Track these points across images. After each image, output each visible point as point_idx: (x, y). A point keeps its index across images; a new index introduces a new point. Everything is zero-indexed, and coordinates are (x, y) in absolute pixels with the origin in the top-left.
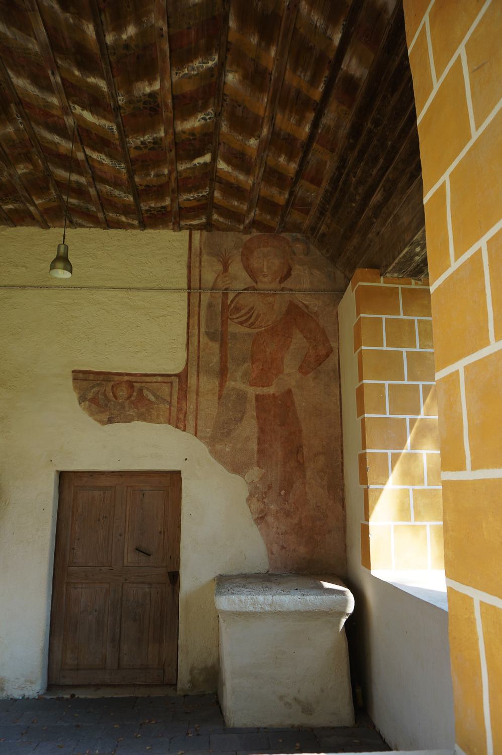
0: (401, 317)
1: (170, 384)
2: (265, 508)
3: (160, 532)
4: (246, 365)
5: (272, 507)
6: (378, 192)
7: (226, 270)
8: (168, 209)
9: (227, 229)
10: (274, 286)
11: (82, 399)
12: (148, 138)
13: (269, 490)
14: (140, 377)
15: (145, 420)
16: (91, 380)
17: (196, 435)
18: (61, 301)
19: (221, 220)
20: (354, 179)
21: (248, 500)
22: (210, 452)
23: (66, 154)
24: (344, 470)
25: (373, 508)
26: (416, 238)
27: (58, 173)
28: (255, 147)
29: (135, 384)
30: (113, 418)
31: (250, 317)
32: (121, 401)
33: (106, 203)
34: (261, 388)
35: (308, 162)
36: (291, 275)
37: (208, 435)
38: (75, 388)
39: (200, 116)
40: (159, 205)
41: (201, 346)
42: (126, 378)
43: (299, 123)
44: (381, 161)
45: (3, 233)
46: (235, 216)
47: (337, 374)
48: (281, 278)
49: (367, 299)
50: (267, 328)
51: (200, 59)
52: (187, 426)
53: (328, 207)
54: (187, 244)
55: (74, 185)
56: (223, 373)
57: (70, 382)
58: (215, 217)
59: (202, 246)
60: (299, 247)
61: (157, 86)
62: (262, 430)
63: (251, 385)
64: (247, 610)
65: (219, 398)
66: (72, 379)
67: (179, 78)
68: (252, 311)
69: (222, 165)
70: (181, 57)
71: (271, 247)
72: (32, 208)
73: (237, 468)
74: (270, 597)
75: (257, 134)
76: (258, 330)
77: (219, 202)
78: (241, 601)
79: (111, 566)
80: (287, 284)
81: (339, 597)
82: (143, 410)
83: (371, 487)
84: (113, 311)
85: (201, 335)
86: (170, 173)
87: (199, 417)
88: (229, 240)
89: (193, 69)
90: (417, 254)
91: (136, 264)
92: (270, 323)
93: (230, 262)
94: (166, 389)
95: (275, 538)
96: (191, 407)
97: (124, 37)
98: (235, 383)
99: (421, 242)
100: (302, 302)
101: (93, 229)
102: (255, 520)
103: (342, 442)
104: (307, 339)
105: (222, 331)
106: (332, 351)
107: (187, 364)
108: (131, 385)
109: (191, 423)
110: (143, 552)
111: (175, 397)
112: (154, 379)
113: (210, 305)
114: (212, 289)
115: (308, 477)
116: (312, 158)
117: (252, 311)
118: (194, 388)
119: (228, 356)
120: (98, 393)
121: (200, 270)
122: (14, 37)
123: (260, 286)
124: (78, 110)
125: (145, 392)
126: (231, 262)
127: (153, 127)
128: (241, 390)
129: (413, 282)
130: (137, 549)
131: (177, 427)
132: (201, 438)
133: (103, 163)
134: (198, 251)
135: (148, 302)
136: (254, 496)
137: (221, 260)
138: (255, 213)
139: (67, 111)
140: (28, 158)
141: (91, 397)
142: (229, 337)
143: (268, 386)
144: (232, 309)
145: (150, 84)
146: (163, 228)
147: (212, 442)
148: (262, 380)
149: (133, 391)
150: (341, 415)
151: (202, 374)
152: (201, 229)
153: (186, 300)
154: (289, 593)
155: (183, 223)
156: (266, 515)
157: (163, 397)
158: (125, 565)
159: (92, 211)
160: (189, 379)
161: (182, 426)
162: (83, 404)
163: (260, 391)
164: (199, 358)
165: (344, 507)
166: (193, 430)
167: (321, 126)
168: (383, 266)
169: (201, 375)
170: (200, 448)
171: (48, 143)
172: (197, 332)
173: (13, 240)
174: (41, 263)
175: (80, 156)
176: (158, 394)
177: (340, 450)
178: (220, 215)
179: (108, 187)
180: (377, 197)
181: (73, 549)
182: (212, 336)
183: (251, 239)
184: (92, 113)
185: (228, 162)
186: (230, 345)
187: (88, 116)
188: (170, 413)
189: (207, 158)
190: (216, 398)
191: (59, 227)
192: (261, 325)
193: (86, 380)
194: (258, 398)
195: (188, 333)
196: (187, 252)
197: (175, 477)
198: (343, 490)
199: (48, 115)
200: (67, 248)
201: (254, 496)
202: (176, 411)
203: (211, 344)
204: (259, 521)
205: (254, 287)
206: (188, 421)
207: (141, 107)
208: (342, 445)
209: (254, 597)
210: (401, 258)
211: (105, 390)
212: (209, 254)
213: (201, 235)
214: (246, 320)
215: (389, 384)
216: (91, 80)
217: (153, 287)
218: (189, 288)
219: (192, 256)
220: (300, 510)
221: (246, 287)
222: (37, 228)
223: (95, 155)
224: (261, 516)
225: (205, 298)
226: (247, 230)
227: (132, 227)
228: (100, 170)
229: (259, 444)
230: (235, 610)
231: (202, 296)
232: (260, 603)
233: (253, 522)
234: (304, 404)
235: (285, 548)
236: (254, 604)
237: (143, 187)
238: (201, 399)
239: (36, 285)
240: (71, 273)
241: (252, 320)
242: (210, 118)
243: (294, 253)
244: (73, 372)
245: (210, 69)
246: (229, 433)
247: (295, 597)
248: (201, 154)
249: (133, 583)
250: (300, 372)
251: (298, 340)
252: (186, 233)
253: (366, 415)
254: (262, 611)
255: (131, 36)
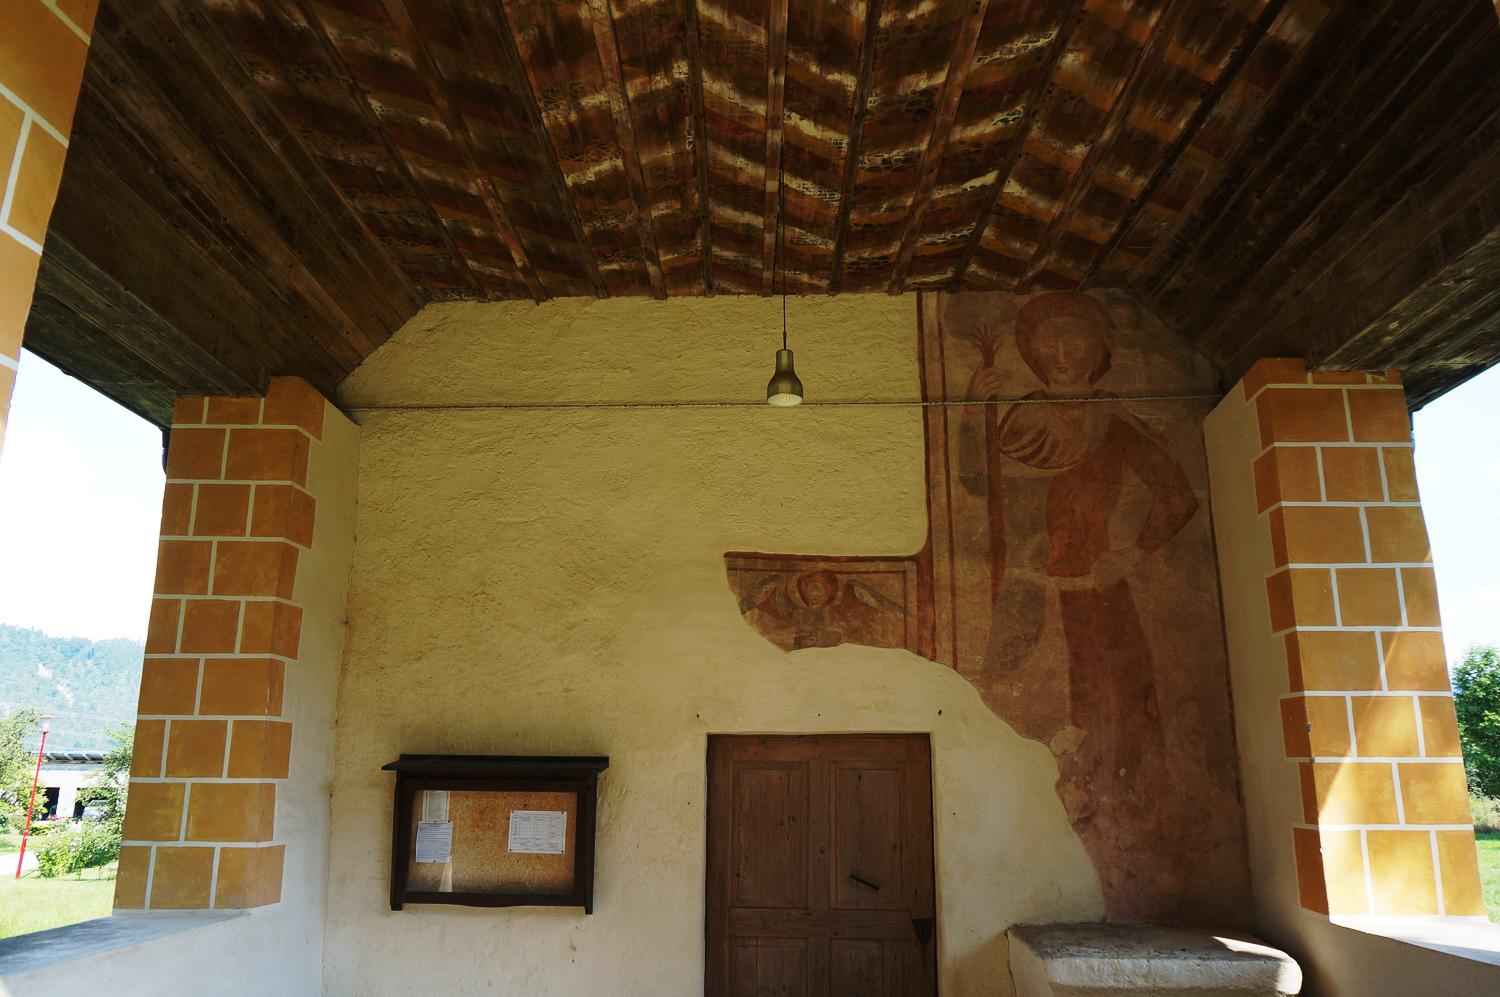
0: (1351, 443)
1: (901, 575)
2: (1092, 801)
3: (894, 847)
4: (1038, 538)
5: (1105, 799)
6: (1309, 223)
7: (988, 362)
8: (891, 260)
9: (990, 286)
10: (1078, 388)
11: (746, 605)
12: (897, 154)
13: (1096, 767)
14: (846, 564)
15: (860, 641)
16: (761, 570)
17: (955, 667)
18: (697, 428)
19: (981, 272)
20: (1257, 201)
21: (1058, 786)
22: (984, 698)
23: (747, 184)
24: (1237, 727)
25: (1324, 799)
26: (1395, 308)
27: (721, 212)
28: (1080, 157)
29: (839, 576)
30: (804, 638)
31: (1041, 448)
32: (815, 606)
33: (788, 254)
34: (1070, 578)
35: (1170, 174)
36: (1110, 366)
37: (979, 667)
38: (733, 585)
39: (1000, 116)
40: (877, 254)
41: (953, 503)
42: (822, 565)
43: (1171, 117)
44: (1322, 173)
45: (587, 309)
46: (1007, 265)
47: (1210, 548)
48: (1093, 373)
49: (1276, 416)
50: (1071, 467)
51: (1026, 38)
52: (938, 650)
53: (1191, 245)
54: (914, 318)
55: (740, 230)
56: (996, 553)
57: (723, 574)
58: (973, 268)
59: (943, 320)
60: (1121, 314)
61: (940, 78)
62: (1076, 657)
63: (1051, 574)
64: (1103, 985)
65: (995, 598)
66: (725, 569)
67: (982, 66)
68: (1044, 437)
69: (1013, 188)
70: (996, 34)
71: (1068, 315)
72: (652, 269)
73: (1035, 727)
74: (1144, 962)
75: (1090, 137)
76: (1055, 472)
77: (988, 244)
78: (1091, 968)
79: (807, 908)
80: (1106, 384)
81: (1270, 964)
82: (857, 623)
83: (1318, 760)
84: (791, 444)
85: (952, 483)
86: (916, 204)
87: (959, 636)
88: (990, 307)
89: (1011, 51)
90: (1390, 333)
91: (824, 357)
92: (1077, 457)
93: (995, 347)
94: (895, 584)
95: (1115, 859)
96: (944, 616)
97: (911, 16)
98: (1022, 571)
99: (1403, 314)
100: (1134, 416)
101: (744, 297)
102: (1075, 825)
103: (1228, 675)
104: (1148, 485)
105: (989, 476)
106: (1198, 506)
107: (930, 537)
108: (830, 577)
109: (945, 645)
110: (865, 883)
111: (913, 598)
112: (872, 567)
113: (965, 429)
114: (968, 398)
115: (1168, 743)
116: (1179, 169)
117: (1044, 437)
118: (945, 581)
119: (1005, 520)
120: (774, 592)
121: (943, 364)
122: (733, 28)
123: (1054, 389)
124: (795, 119)
125: (858, 591)
126: (998, 348)
127: (912, 137)
128: (1032, 584)
129: (1369, 377)
130: (853, 877)
131: (920, 653)
132: (965, 674)
133: (804, 195)
134: (936, 328)
135: (851, 426)
136: (1069, 780)
137: (979, 343)
138: (1048, 261)
139: (774, 122)
140: (679, 193)
141: (762, 601)
142: (1004, 486)
143: (1082, 575)
144: (1005, 436)
145: (930, 77)
146: (871, 291)
147: (985, 680)
148: (1071, 562)
149: (837, 590)
150: (1223, 627)
151: (960, 555)
152: (939, 290)
153: (921, 420)
154: (1171, 955)
155: (909, 281)
156: (1094, 814)
157: (890, 598)
158: (833, 905)
159: (755, 268)
160: (935, 564)
161: (928, 651)
162: (748, 613)
163: (1067, 584)
164: (950, 526)
165: (1240, 799)
166: (949, 658)
167: (1208, 118)
168: (1313, 353)
169: (957, 558)
170: (963, 693)
171: (722, 169)
172: (943, 479)
173: (605, 322)
174: (657, 361)
175: (772, 186)
176: (882, 593)
177: (1226, 694)
178: (983, 265)
179: (797, 230)
180: (1305, 231)
181: (738, 875)
182: (972, 485)
183: (1030, 302)
184: (816, 122)
185: (1024, 182)
186: (1006, 501)
187: (808, 127)
188: (906, 627)
189: (990, 178)
190: (989, 598)
191: (683, 296)
192: (1061, 462)
193: (750, 570)
194: (1065, 597)
195: (928, 481)
196: (915, 331)
197: (919, 746)
198: (1236, 767)
199: (739, 128)
200: (790, 353)
201: (1069, 780)
202: (916, 623)
203: (970, 500)
204: (1081, 826)
205: (1043, 391)
206: (939, 643)
207: (903, 111)
208: (1229, 683)
209: (1116, 961)
210: (1357, 341)
211: (786, 588)
212: (955, 334)
213: (938, 298)
214: (1033, 455)
215: (1337, 570)
216: (835, 77)
217: (861, 399)
218: (925, 398)
219: (925, 338)
220: (1157, 803)
221: (1029, 391)
222: (646, 298)
223: (794, 184)
224: (1084, 816)
225: (955, 415)
226: (1024, 288)
227: (816, 290)
228: (794, 204)
229: (1073, 682)
230: (1081, 984)
231: (949, 412)
232: (1127, 972)
233: (1070, 828)
234: (1151, 607)
235: (1134, 876)
236: (1115, 975)
237: (860, 228)
238: (960, 602)
239: (651, 400)
240: (802, 396)
241: (1044, 453)
242: (1013, 120)
243: (1113, 325)
244: (727, 555)
245: (1041, 50)
246: (1015, 663)
247: (1191, 963)
248: (981, 172)
249: (849, 939)
250: (1141, 547)
251: (1132, 487)
252: (912, 297)
253: (1299, 628)
254: (1131, 987)
255: (923, 15)
